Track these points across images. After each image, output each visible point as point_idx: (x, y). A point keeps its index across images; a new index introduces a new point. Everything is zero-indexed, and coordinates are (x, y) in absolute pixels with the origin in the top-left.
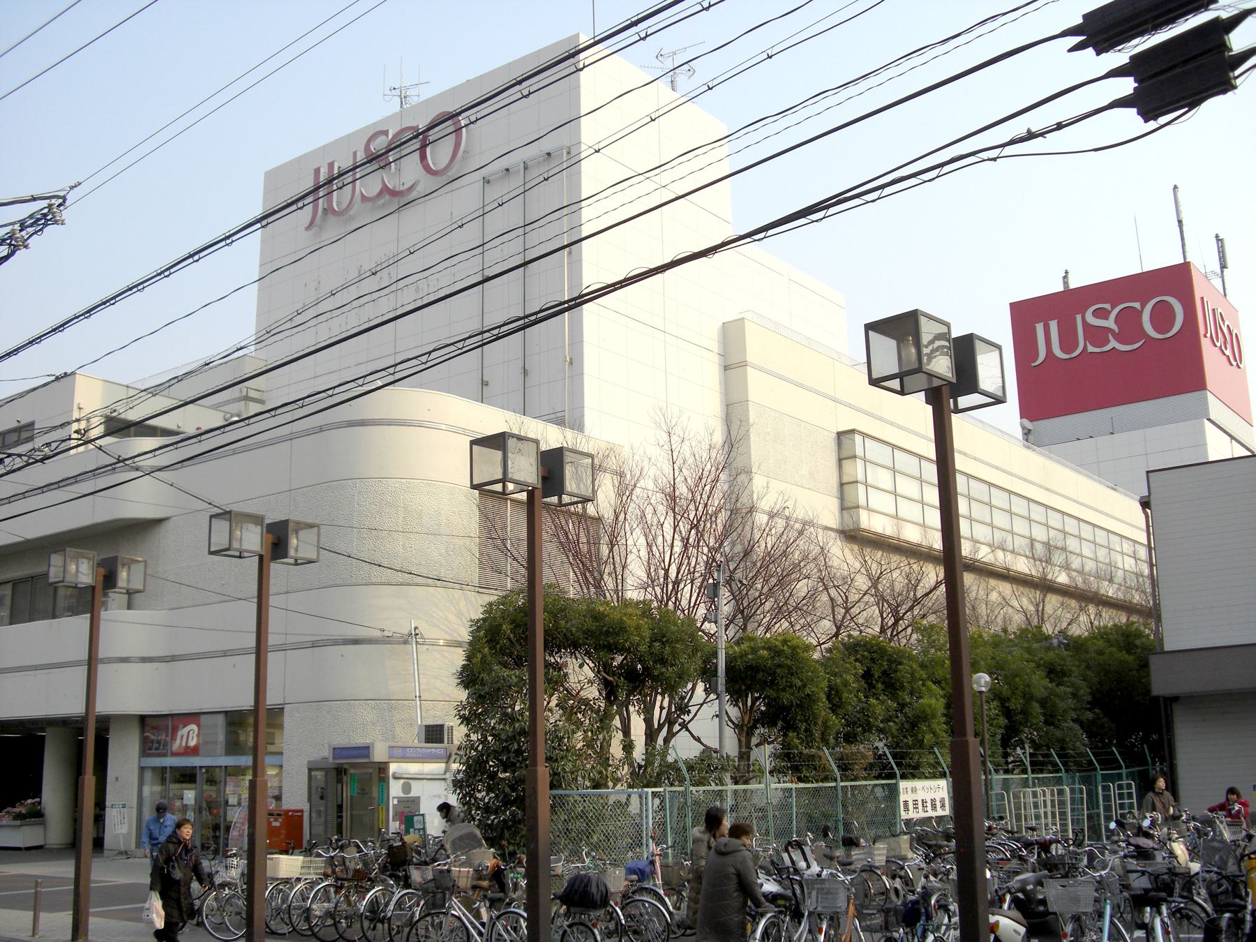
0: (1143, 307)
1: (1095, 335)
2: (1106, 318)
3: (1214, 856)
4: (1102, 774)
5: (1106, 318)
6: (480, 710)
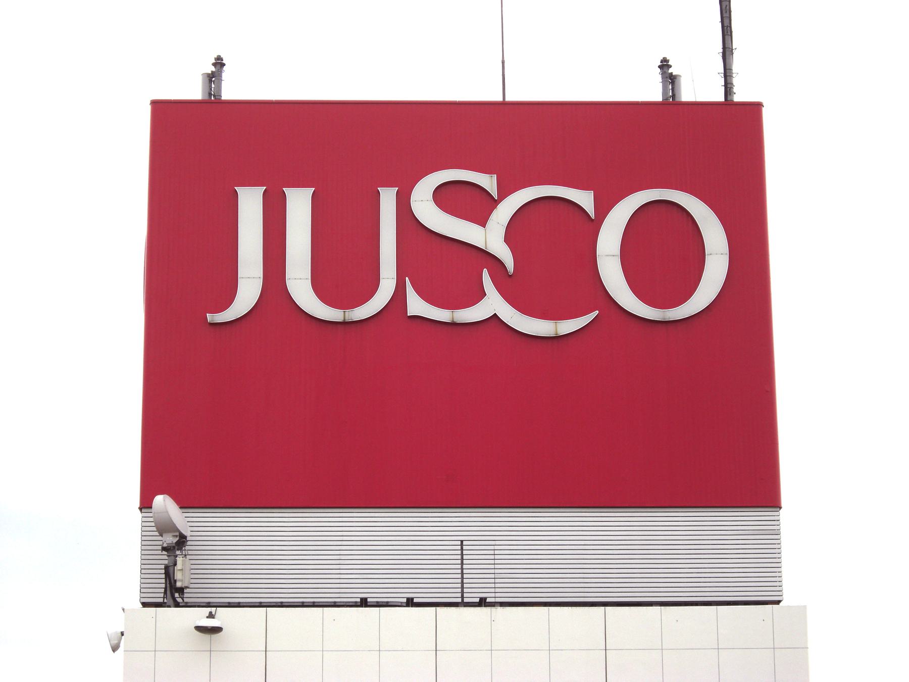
0: (604, 207)
2: (482, 220)
5: (482, 220)
6: (213, 98)
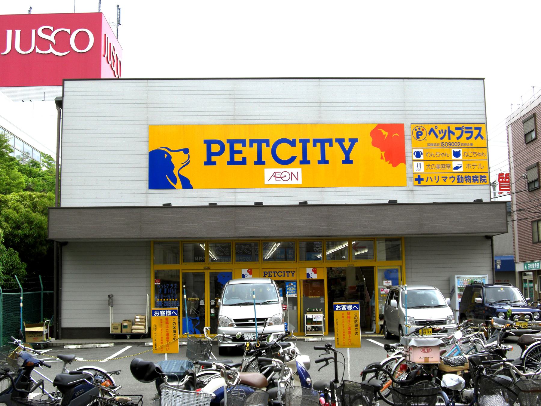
0: (72, 32)
1: (42, 43)
2: (50, 35)
3: (479, 385)
4: (4, 295)
5: (50, 35)
